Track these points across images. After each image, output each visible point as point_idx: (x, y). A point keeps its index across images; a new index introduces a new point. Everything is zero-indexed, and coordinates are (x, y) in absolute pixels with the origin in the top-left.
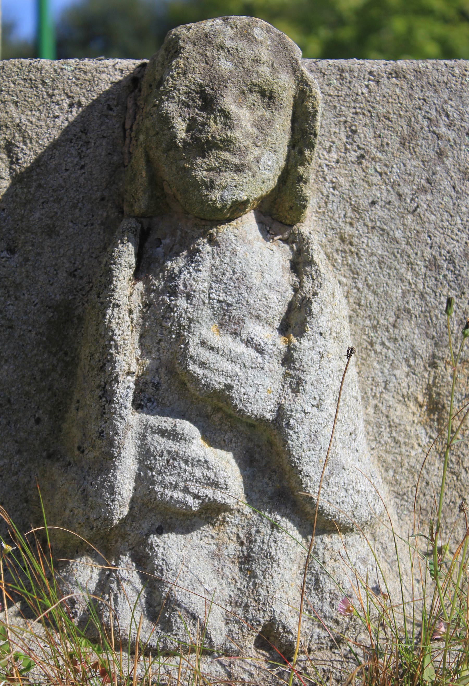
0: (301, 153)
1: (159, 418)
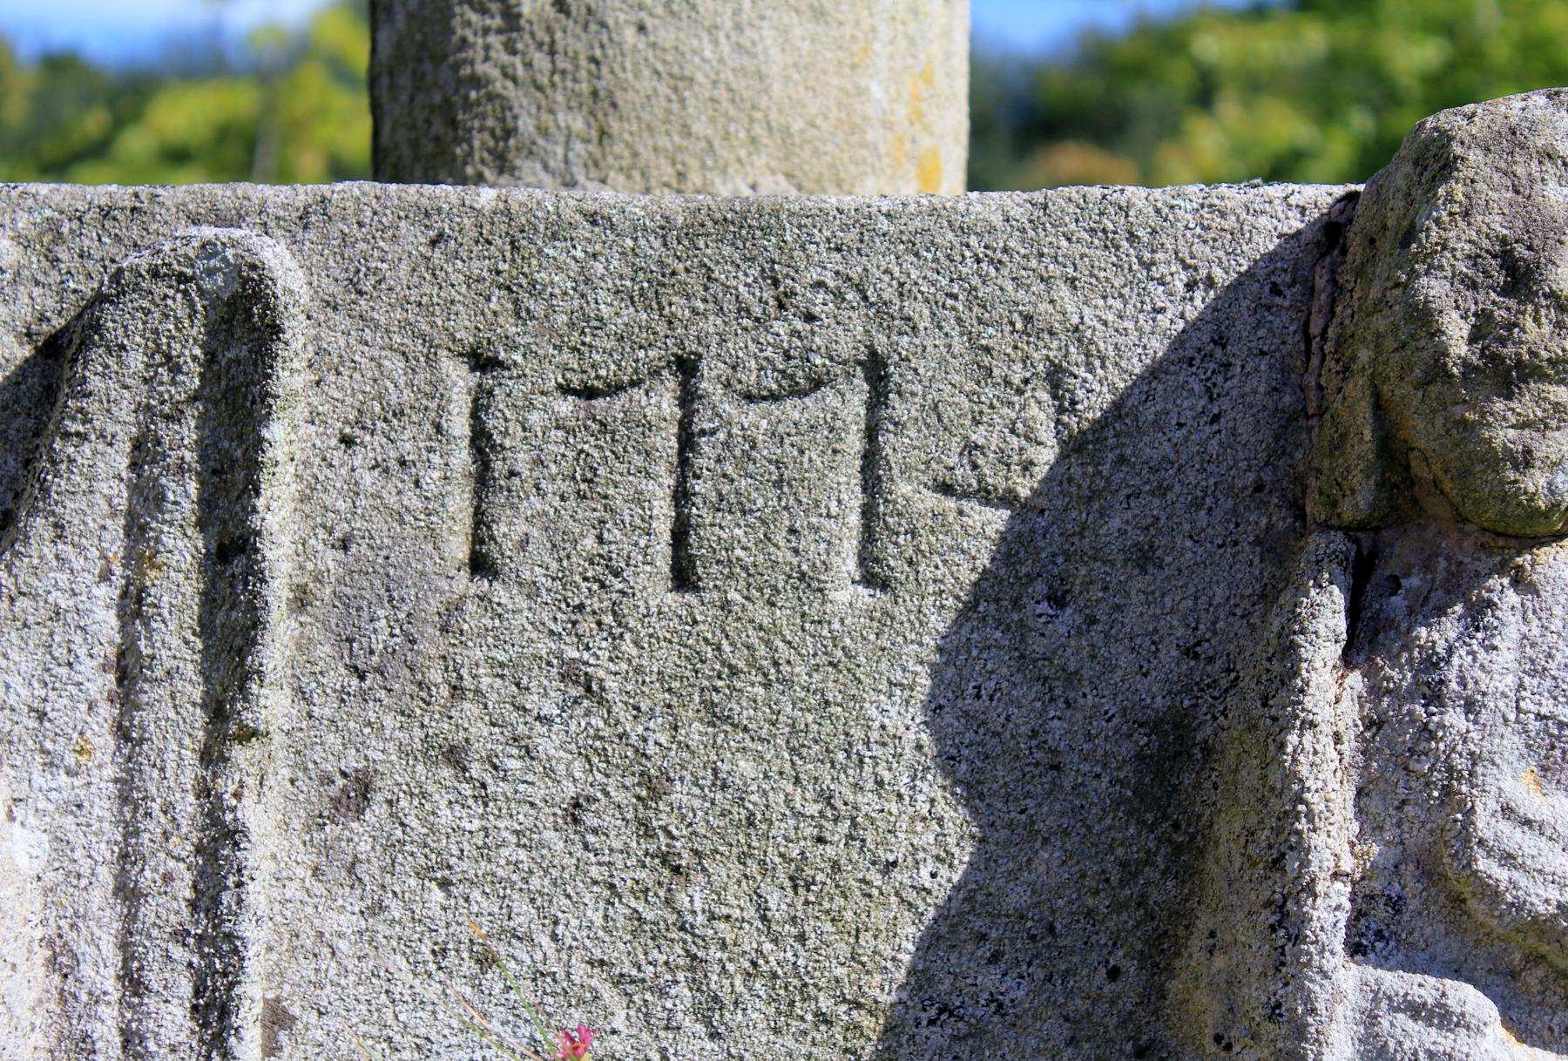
1: (1406, 975)
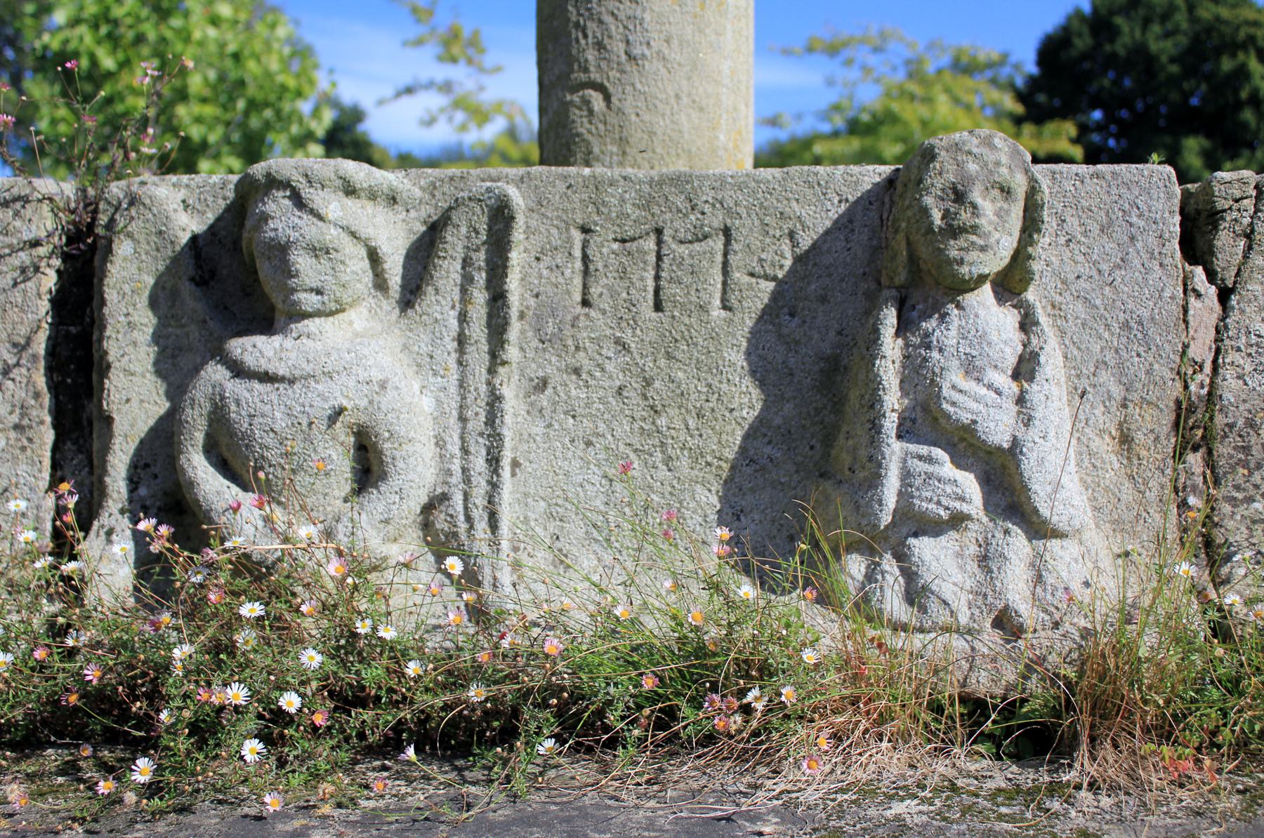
0: (1031, 236)
